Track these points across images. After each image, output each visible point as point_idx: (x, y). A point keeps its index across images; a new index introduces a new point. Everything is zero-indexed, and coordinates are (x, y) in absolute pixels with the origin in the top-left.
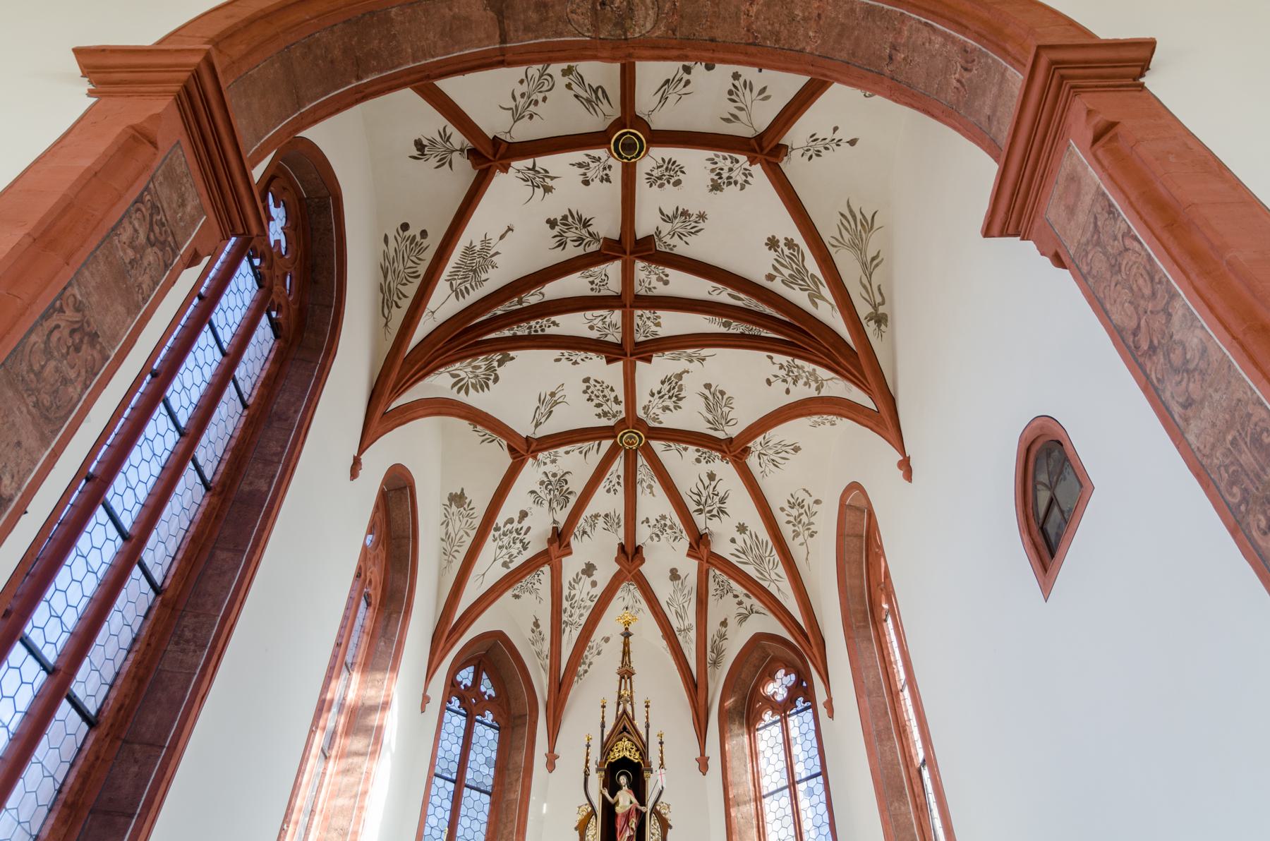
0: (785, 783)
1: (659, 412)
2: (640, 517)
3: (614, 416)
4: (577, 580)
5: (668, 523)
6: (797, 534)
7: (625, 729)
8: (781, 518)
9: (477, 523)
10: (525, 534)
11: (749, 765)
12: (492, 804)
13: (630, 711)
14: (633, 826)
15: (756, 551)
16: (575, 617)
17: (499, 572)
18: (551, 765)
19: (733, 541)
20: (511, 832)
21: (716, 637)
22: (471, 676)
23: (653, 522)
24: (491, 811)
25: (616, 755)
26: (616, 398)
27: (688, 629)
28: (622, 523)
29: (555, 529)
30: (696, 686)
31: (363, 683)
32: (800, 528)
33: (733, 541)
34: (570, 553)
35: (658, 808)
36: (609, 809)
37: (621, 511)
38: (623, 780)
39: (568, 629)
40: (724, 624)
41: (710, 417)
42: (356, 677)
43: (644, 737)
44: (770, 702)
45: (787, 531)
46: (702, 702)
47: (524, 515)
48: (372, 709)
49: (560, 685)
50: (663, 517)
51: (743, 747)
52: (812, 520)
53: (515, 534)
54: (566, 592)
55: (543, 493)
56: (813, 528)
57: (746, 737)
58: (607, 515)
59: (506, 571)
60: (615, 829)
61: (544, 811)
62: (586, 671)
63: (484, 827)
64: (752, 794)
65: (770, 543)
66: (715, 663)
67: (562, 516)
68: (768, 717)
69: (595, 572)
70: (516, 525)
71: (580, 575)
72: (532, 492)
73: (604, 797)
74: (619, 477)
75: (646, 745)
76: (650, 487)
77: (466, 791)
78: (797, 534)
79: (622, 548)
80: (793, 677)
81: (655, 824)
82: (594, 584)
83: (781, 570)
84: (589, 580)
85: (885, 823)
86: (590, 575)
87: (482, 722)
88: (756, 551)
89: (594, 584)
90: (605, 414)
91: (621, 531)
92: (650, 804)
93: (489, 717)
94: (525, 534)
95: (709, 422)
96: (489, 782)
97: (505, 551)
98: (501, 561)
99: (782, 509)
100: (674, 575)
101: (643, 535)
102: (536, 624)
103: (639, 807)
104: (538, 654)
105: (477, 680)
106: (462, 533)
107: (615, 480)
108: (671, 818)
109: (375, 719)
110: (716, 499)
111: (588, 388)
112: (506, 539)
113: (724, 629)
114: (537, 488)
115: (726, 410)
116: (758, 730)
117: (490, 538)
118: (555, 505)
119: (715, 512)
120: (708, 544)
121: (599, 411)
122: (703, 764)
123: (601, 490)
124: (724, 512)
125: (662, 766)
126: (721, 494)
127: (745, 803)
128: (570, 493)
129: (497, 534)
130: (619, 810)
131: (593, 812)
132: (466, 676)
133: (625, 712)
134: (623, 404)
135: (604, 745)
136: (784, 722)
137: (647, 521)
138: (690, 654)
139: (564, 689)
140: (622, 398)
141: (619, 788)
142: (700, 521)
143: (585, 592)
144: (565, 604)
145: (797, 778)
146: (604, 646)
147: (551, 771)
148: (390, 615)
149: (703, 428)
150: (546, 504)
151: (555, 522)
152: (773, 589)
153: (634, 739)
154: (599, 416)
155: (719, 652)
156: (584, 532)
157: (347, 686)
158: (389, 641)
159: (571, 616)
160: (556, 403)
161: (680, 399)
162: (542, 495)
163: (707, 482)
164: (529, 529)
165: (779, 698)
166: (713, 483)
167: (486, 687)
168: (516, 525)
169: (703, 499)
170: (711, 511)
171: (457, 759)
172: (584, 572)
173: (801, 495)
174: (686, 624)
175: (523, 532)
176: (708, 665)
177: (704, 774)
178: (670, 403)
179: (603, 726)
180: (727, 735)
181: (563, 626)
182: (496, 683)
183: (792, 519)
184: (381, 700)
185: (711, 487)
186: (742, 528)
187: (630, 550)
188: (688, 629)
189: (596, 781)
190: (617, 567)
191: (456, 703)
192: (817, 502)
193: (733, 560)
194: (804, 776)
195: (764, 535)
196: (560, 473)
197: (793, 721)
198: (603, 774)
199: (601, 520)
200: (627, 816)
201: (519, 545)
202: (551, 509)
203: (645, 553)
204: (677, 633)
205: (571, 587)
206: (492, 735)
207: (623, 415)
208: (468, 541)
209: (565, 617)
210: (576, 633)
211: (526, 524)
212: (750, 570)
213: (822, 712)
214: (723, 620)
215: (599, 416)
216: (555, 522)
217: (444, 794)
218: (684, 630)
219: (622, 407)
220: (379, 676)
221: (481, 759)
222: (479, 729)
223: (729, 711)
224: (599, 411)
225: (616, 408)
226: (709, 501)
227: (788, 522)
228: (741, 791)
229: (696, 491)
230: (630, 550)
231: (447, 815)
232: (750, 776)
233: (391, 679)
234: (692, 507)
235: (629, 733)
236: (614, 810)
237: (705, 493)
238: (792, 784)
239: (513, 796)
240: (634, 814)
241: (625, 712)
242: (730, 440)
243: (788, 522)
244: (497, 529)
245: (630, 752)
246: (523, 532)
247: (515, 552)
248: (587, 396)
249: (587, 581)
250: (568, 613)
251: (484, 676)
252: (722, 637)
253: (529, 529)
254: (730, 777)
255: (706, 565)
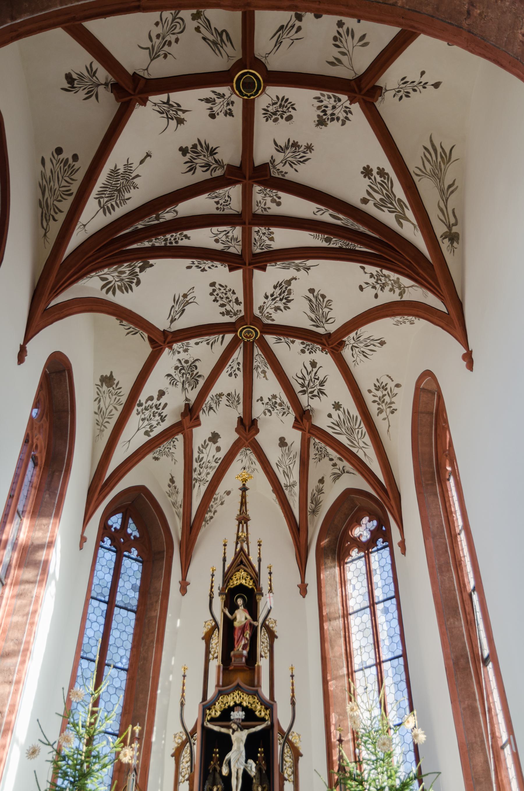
0: (367, 603)
1: (272, 311)
2: (256, 396)
3: (235, 314)
4: (204, 446)
5: (278, 401)
6: (380, 411)
7: (242, 562)
8: (368, 398)
9: (124, 399)
10: (163, 409)
11: (339, 590)
12: (137, 619)
13: (246, 549)
14: (248, 636)
15: (347, 424)
16: (203, 475)
17: (141, 440)
18: (183, 590)
19: (330, 416)
20: (152, 641)
21: (315, 491)
22: (120, 521)
23: (266, 400)
24: (136, 625)
25: (235, 582)
26: (237, 299)
27: (293, 485)
28: (241, 401)
29: (187, 405)
30: (299, 529)
31: (32, 527)
32: (383, 406)
33: (330, 416)
34: (199, 424)
35: (267, 623)
36: (229, 623)
37: (240, 391)
38: (240, 602)
39: (197, 485)
40: (321, 481)
41: (313, 316)
42: (26, 522)
43: (257, 569)
44: (357, 543)
45: (373, 408)
46: (303, 542)
47: (161, 393)
48: (40, 547)
49: (191, 528)
50: (274, 397)
51: (334, 577)
52: (393, 400)
53: (154, 409)
54: (196, 455)
55: (177, 376)
56: (394, 406)
57: (337, 569)
58: (229, 395)
59: (147, 438)
60: (233, 639)
61: (179, 621)
62: (211, 518)
63: (131, 638)
64: (341, 612)
65: (359, 418)
66: (314, 512)
67: (193, 395)
68: (354, 553)
69: (219, 440)
70: (155, 402)
71: (207, 442)
72: (169, 375)
73: (225, 615)
74: (239, 364)
75: (258, 575)
76: (264, 372)
77: (116, 610)
78: (380, 411)
79: (241, 421)
80: (375, 523)
81: (264, 635)
82: (218, 449)
83: (367, 439)
84: (214, 446)
85: (442, 634)
86: (215, 442)
87: (129, 557)
88: (347, 424)
89: (218, 449)
90: (228, 313)
91: (241, 407)
92: (261, 620)
93: (134, 553)
94: (163, 409)
95: (312, 320)
96: (135, 603)
97: (146, 422)
98: (144, 430)
99: (370, 391)
100: (282, 442)
101: (258, 410)
102: (172, 481)
103: (252, 622)
104: (174, 504)
105: (124, 524)
106: (111, 407)
107: (235, 367)
108: (277, 630)
109: (42, 555)
110: (317, 382)
111: (214, 291)
112: (147, 413)
113: (321, 485)
114: (172, 372)
115: (326, 310)
116: (346, 563)
117: (134, 412)
118: (187, 386)
119: (316, 393)
120: (309, 418)
121: (223, 310)
122: (303, 590)
123: (224, 375)
124: (323, 393)
125: (270, 591)
126: (321, 378)
127: (335, 619)
128: (200, 376)
129: (140, 409)
130: (236, 624)
131: (216, 626)
132: (116, 521)
133: (242, 549)
134: (242, 305)
135: (225, 575)
136: (367, 557)
137: (261, 399)
138: (294, 505)
139: (194, 531)
140: (241, 299)
141: (237, 607)
142: (304, 399)
143: (211, 456)
144: (195, 465)
145: (376, 600)
146: (226, 498)
147: (183, 595)
148: (53, 473)
149: (307, 325)
150: (180, 385)
151: (187, 399)
152: (361, 455)
153: (249, 570)
154: (223, 314)
155: (317, 503)
156: (211, 408)
157: (19, 530)
158: (53, 493)
159: (200, 474)
160: (188, 303)
161: (289, 301)
162: (177, 378)
163: (309, 368)
164: (166, 405)
165: (364, 539)
166: (315, 370)
167: (132, 530)
168: (155, 402)
169: (307, 382)
170: (311, 392)
171: (109, 586)
172: (210, 439)
173: (385, 380)
174: (291, 481)
175: (161, 407)
176: (308, 513)
177: (304, 597)
178: (281, 305)
179: (224, 560)
180: (323, 567)
181: (194, 482)
182: (138, 529)
183: (377, 399)
184: (47, 540)
185: (313, 373)
186: (337, 406)
187: (247, 423)
188: (293, 485)
189: (218, 602)
190: (236, 436)
191: (107, 542)
192: (398, 386)
193: (330, 431)
194: (381, 599)
195: (355, 412)
196: (191, 360)
197: (374, 557)
198: (224, 597)
199: (224, 398)
200: (243, 629)
201: (158, 418)
202: (184, 389)
203: (260, 425)
204: (284, 488)
205: (200, 451)
206: (136, 567)
207: (243, 314)
208: (116, 415)
209: (195, 475)
210: (204, 488)
211: (163, 400)
212: (343, 439)
213: (397, 549)
214: (321, 478)
215: (223, 314)
216: (187, 399)
217: (98, 612)
218: (290, 486)
219: (242, 307)
220: (44, 521)
221: (128, 586)
222: (126, 562)
223: (324, 549)
224: (223, 310)
225: (236, 308)
226: (311, 384)
227: (374, 402)
228: (332, 609)
229: (300, 375)
230: (247, 423)
231: (102, 629)
232: (339, 599)
233: (54, 524)
234: (297, 388)
235: (245, 565)
236: (233, 624)
237: (308, 378)
238: (372, 605)
239: (153, 614)
240: (248, 628)
241: (242, 549)
242: (329, 335)
243: (374, 402)
244: (140, 405)
245: (246, 580)
246: (161, 407)
247: (154, 423)
248: (213, 298)
249: (212, 447)
250: (198, 472)
251: (131, 521)
252: (320, 491)
253: (166, 405)
254: (324, 599)
255: (308, 435)
